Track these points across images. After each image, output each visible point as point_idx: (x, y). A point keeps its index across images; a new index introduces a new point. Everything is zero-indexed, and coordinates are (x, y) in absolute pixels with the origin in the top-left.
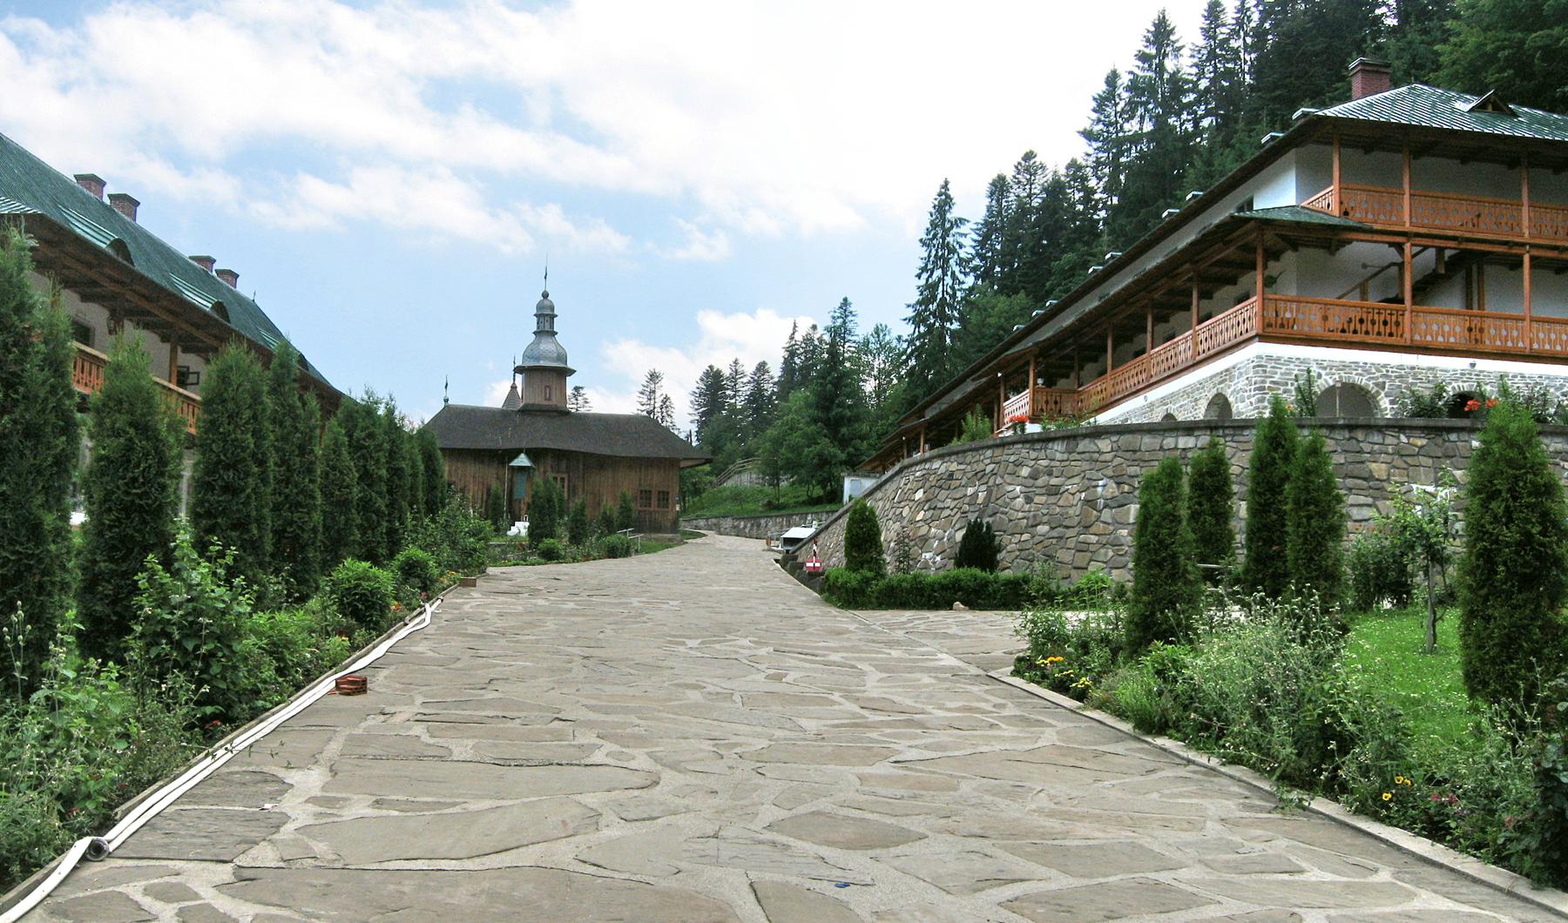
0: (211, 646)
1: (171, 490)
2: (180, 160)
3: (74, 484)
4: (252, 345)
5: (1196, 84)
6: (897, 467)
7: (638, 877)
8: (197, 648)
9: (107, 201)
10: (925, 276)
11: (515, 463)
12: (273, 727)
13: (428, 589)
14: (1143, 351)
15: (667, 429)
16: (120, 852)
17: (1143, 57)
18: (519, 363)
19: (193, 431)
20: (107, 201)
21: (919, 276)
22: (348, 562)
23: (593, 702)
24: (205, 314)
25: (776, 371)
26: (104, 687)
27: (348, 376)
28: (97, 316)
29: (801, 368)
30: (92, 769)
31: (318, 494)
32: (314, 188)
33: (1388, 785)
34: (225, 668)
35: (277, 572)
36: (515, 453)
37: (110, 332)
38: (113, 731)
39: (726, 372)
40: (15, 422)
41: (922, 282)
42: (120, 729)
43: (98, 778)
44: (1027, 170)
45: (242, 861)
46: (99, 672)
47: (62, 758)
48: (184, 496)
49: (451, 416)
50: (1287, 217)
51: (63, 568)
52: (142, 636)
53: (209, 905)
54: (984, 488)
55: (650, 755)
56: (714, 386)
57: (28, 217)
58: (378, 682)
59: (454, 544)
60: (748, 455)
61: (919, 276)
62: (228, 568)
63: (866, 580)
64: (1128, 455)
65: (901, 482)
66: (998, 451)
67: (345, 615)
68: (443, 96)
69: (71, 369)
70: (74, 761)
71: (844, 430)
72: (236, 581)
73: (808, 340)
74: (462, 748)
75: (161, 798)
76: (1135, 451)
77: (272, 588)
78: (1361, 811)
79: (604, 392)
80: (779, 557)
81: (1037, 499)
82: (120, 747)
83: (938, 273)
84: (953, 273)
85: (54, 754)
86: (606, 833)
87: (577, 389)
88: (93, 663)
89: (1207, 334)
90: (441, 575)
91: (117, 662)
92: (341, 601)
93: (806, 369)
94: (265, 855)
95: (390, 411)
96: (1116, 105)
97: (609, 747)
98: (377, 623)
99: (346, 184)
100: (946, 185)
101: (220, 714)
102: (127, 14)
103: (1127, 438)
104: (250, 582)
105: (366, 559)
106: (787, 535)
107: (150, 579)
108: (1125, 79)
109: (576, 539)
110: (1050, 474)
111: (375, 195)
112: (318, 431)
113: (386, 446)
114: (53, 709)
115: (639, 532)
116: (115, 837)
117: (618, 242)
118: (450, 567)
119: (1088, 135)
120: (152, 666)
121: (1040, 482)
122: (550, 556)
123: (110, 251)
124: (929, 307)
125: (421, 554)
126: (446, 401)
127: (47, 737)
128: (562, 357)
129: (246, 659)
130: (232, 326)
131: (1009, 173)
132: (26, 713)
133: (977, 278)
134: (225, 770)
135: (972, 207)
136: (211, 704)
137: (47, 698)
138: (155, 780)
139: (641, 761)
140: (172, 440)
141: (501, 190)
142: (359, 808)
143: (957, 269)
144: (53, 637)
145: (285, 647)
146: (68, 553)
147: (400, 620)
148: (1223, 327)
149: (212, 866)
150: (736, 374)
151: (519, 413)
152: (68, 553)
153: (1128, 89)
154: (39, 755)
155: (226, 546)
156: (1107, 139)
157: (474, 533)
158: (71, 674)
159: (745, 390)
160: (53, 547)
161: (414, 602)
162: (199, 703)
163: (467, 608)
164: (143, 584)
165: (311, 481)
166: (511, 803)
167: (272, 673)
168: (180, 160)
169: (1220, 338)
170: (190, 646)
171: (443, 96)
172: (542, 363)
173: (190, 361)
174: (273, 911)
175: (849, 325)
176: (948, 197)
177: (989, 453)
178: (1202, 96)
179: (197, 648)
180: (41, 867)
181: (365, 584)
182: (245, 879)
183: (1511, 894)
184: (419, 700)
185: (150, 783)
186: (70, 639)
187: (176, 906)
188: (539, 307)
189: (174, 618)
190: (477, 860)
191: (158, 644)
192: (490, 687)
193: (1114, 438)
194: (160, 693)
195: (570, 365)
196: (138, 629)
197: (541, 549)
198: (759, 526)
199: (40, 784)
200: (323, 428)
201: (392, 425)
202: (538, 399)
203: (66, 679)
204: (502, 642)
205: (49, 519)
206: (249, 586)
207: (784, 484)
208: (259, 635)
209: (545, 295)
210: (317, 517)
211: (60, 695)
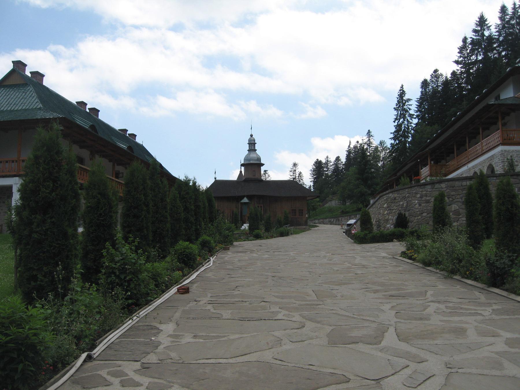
0: (130, 277)
1: (114, 218)
2: (114, 94)
3: (79, 217)
4: (143, 161)
5: (498, 39)
6: (378, 197)
7: (298, 365)
8: (125, 277)
9: (88, 111)
10: (397, 121)
11: (243, 201)
12: (154, 307)
13: (211, 252)
14: (466, 150)
15: (301, 185)
16: (98, 358)
17: (475, 31)
18: (243, 162)
19: (122, 195)
20: (88, 111)
21: (394, 122)
22: (181, 242)
23: (277, 294)
24: (125, 150)
25: (343, 159)
26: (91, 294)
27: (178, 171)
28: (85, 154)
29: (354, 158)
30: (87, 326)
31: (169, 217)
32: (163, 101)
33: (468, 270)
34: (136, 285)
35: (154, 247)
36: (242, 197)
37: (91, 159)
38: (95, 311)
39: (324, 161)
40: (57, 195)
41: (396, 124)
42: (97, 310)
43: (89, 329)
44: (436, 76)
45: (144, 360)
46: (89, 288)
47: (76, 322)
48: (119, 220)
49: (218, 184)
50: (509, 102)
51: (76, 249)
52: (105, 274)
53: (132, 379)
54: (405, 202)
55: (300, 315)
56: (319, 166)
57: (59, 118)
58: (193, 289)
59: (220, 234)
60: (334, 193)
61: (394, 122)
62: (136, 246)
63: (367, 235)
64: (451, 188)
65: (380, 201)
66: (409, 189)
67: (180, 263)
68: (210, 62)
69: (77, 174)
70: (81, 323)
71: (369, 182)
72: (139, 251)
73: (355, 147)
74: (226, 314)
75: (113, 336)
76: (453, 187)
77: (152, 253)
78: (463, 277)
79: (276, 171)
80: (344, 231)
81: (423, 205)
82: (98, 317)
83: (402, 120)
84: (407, 120)
85: (73, 320)
86: (284, 347)
87: (265, 171)
88: (87, 285)
89: (485, 144)
90: (216, 246)
91: (96, 284)
92: (179, 258)
93: (355, 158)
94: (152, 358)
95: (195, 183)
96: (467, 50)
97: (284, 312)
98: (192, 265)
99: (175, 98)
100: (402, 87)
101: (135, 303)
102: (93, 41)
103: (451, 182)
104: (144, 251)
105: (187, 241)
106: (348, 223)
107: (107, 252)
108: (469, 40)
109: (267, 230)
110: (426, 196)
111: (185, 102)
112: (168, 193)
113: (193, 197)
114: (73, 303)
115: (292, 226)
116: (97, 351)
117: (278, 113)
118: (219, 243)
119: (457, 62)
120: (109, 285)
121: (423, 199)
122: (258, 237)
123: (90, 129)
124: (400, 133)
125: (208, 238)
126: (215, 178)
127: (71, 314)
128: (259, 159)
129: (144, 281)
130: (135, 155)
131: (428, 78)
132: (63, 305)
133: (419, 119)
134: (137, 325)
135: (414, 94)
136: (131, 299)
137: (71, 299)
138: (111, 329)
139: (297, 317)
140: (114, 199)
141: (233, 96)
142: (188, 339)
143: (409, 118)
144: (72, 275)
145: (158, 276)
146: (77, 243)
147: (201, 264)
148: (490, 141)
149: (133, 363)
150: (327, 162)
151: (242, 181)
152: (77, 243)
153: (470, 44)
154: (68, 321)
155: (135, 238)
156: (464, 62)
157: (228, 229)
158: (79, 289)
159: (332, 168)
160: (71, 241)
161: (206, 257)
162: (127, 299)
163: (226, 258)
164: (105, 254)
165: (166, 212)
166: (246, 335)
167: (153, 286)
168: (114, 94)
169: (490, 145)
170: (122, 277)
171: (210, 62)
172: (251, 162)
173: (120, 169)
174: (156, 380)
175: (371, 140)
176: (403, 91)
177: (407, 190)
178: (501, 44)
179: (125, 277)
180: (69, 364)
181: (187, 251)
182: (145, 368)
183: (483, 289)
184: (209, 295)
185: (109, 331)
186: (79, 276)
187: (119, 379)
188: (249, 140)
189: (117, 266)
190: (234, 359)
191: (111, 277)
192: (237, 289)
193: (446, 183)
194: (112, 295)
195: (262, 162)
196: (103, 271)
197: (254, 234)
198: (339, 220)
199: (69, 332)
200: (169, 191)
201: (195, 188)
202: (251, 176)
203: (77, 291)
204: (240, 271)
205: (70, 231)
206: (144, 253)
207: (348, 204)
208: (148, 272)
209: (251, 136)
210: (168, 225)
211: (76, 297)
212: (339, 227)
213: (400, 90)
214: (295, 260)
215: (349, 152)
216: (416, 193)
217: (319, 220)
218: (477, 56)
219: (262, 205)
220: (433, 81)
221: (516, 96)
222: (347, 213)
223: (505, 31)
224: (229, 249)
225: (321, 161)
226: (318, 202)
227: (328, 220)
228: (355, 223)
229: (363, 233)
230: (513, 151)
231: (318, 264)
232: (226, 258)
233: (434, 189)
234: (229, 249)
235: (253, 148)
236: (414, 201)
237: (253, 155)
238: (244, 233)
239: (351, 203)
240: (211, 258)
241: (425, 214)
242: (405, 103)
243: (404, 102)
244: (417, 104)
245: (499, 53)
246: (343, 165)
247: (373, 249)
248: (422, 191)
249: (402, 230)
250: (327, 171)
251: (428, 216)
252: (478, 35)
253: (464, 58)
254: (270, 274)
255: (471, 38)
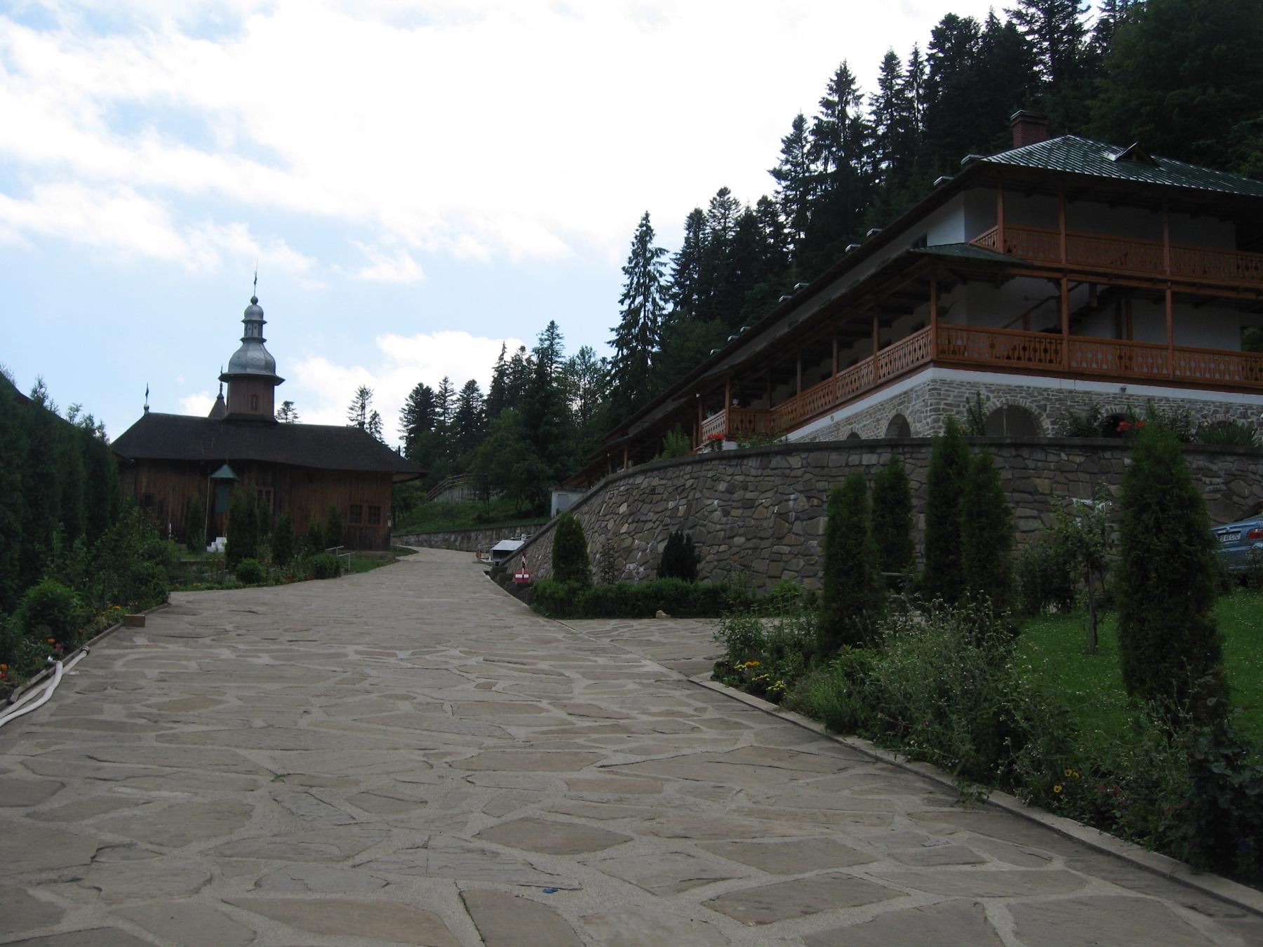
5: (874, 130)
6: (602, 483)
10: (627, 302)
13: (67, 638)
14: (830, 375)
18: (226, 371)
21: (622, 302)
25: (485, 388)
29: (510, 388)
33: (1059, 778)
36: (217, 465)
39: (436, 390)
41: (625, 307)
44: (722, 205)
49: (154, 427)
50: (957, 253)
54: (684, 501)
56: (423, 402)
60: (457, 471)
61: (622, 302)
63: (571, 591)
66: (697, 467)
73: (517, 361)
76: (823, 468)
78: (1035, 803)
79: (316, 395)
80: (489, 569)
81: (734, 512)
83: (639, 299)
84: (654, 299)
87: (287, 404)
89: (887, 360)
93: (515, 387)
96: (803, 147)
103: (817, 455)
106: (498, 547)
108: (810, 124)
109: (280, 558)
110: (745, 489)
119: (778, 174)
121: (736, 496)
122: (250, 579)
124: (630, 332)
125: (60, 589)
126: (146, 408)
128: (271, 365)
131: (706, 208)
133: (676, 305)
135: (671, 239)
143: (657, 296)
148: (901, 353)
151: (222, 419)
153: (813, 132)
159: (455, 407)
172: (249, 371)
176: (649, 228)
177: (689, 468)
178: (881, 142)
183: (1172, 879)
188: (248, 313)
193: (804, 456)
195: (279, 373)
197: (243, 571)
198: (469, 538)
202: (246, 409)
207: (493, 499)
209: (254, 301)
212: (472, 556)
213: (641, 226)
214: (365, 685)
215: (501, 371)
216: (716, 480)
217: (418, 535)
218: (826, 164)
219: (272, 490)
220: (715, 216)
221: (972, 241)
222: (495, 524)
223: (892, 114)
224: (143, 625)
225: (428, 389)
226: (417, 489)
227: (441, 536)
228: (522, 551)
229: (566, 587)
230: (962, 384)
231: (447, 708)
232: (118, 666)
233: (768, 472)
234: (143, 625)
235: (256, 335)
236: (709, 502)
237: (254, 354)
238: (213, 561)
239: (503, 498)
240: (60, 665)
241: (739, 540)
242: (652, 257)
243: (649, 255)
244: (675, 266)
245: (876, 164)
246: (484, 401)
247: (605, 642)
248: (732, 475)
249: (679, 585)
250: (444, 413)
251: (750, 544)
252: (833, 115)
253: (795, 165)
254: (261, 758)
255: (816, 118)
